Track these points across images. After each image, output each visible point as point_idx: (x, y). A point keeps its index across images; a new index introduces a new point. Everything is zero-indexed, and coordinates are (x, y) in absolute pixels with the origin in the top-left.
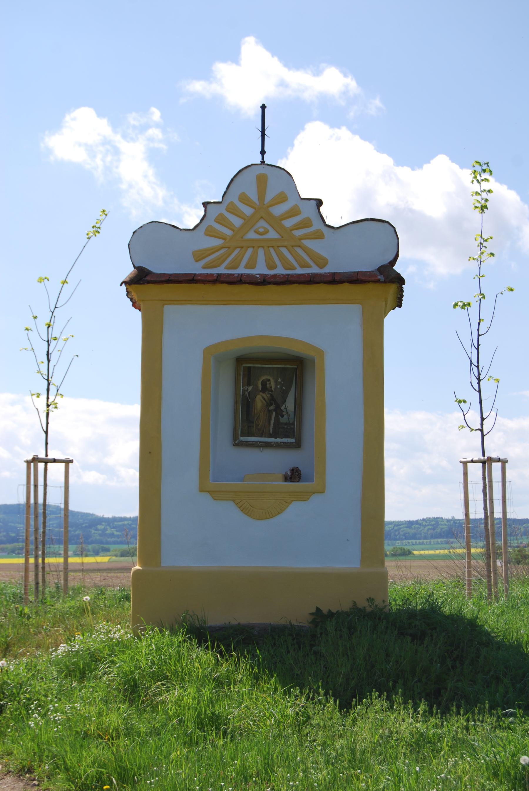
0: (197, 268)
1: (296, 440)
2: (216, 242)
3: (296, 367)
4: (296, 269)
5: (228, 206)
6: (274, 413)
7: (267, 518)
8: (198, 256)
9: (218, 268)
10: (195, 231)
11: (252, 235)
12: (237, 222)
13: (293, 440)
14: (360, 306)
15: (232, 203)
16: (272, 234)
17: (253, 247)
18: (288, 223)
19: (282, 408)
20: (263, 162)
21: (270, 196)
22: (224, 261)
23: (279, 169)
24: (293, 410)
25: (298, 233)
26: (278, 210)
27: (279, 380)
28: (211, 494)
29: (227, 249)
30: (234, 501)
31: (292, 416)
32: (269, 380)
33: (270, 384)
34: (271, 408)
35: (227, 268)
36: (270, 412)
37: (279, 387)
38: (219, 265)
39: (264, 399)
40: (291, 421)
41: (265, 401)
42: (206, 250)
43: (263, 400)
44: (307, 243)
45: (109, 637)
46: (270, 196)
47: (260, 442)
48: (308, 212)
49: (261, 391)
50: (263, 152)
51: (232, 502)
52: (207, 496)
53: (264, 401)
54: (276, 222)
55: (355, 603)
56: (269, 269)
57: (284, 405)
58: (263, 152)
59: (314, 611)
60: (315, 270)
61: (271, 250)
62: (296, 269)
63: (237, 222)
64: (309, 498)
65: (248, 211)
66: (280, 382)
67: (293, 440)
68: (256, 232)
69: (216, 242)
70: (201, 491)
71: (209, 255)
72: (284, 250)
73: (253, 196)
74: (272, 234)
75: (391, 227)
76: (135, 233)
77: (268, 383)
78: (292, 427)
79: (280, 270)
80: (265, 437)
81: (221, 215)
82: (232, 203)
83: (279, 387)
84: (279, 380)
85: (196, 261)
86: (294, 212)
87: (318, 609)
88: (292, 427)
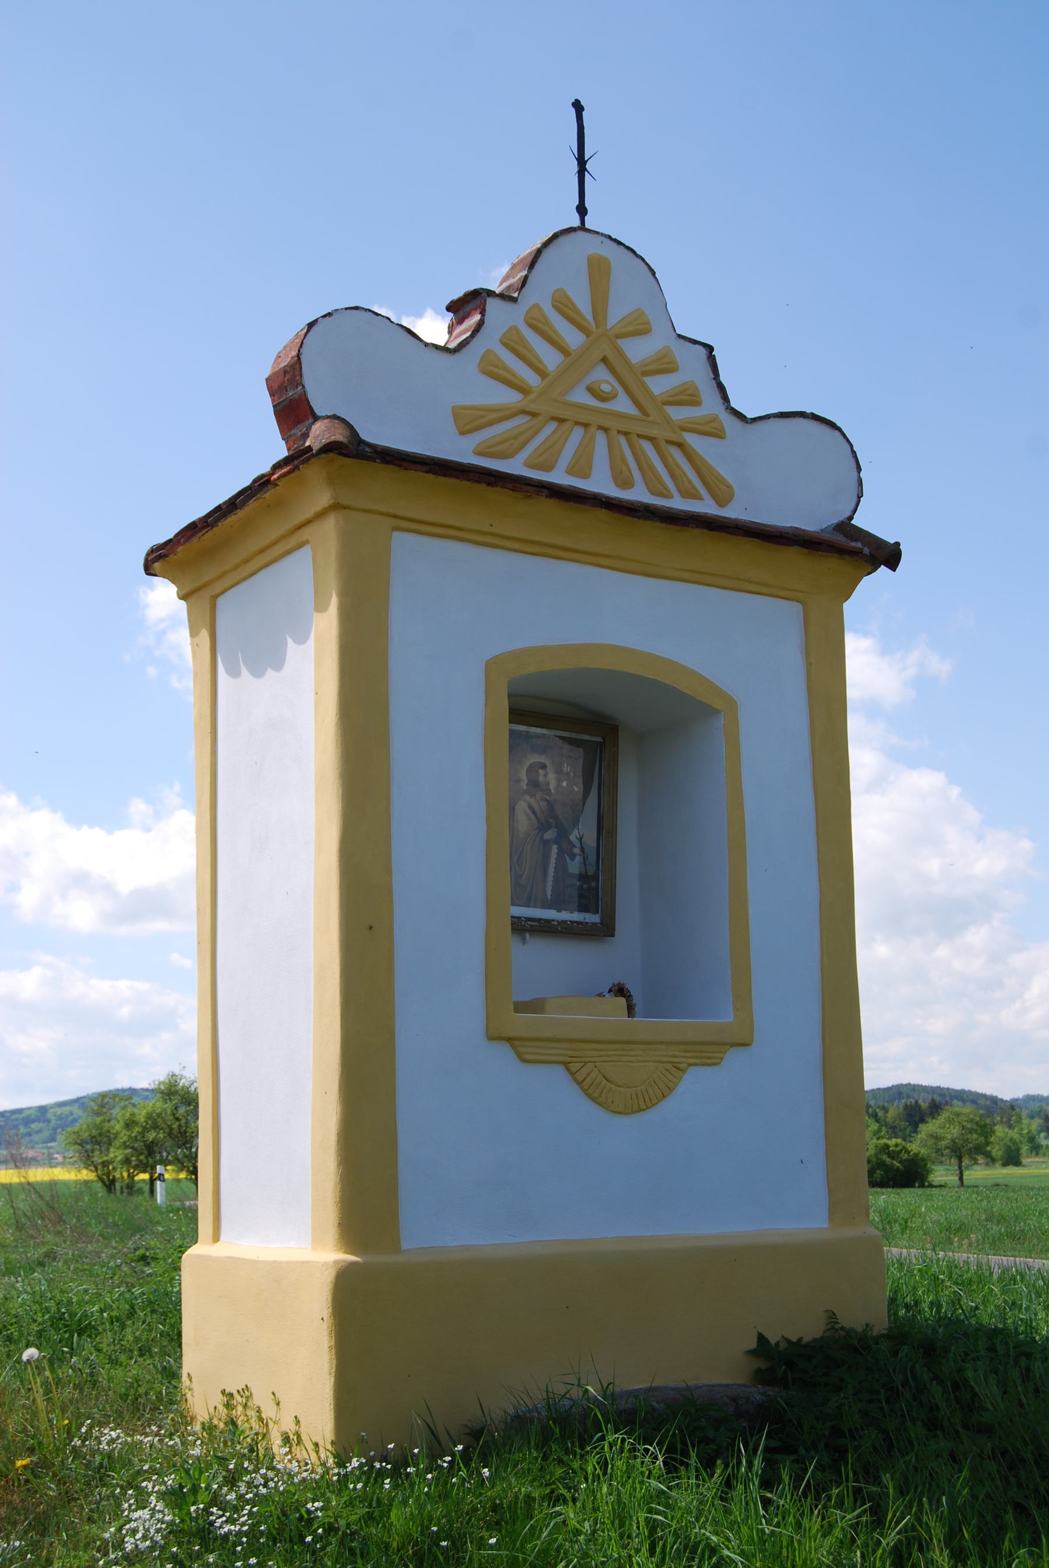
0: (461, 451)
1: (602, 918)
2: (509, 397)
3: (599, 739)
4: (672, 497)
5: (529, 311)
6: (555, 848)
7: (641, 1110)
8: (468, 421)
9: (507, 461)
10: (457, 355)
11: (581, 396)
12: (551, 359)
13: (593, 918)
14: (796, 608)
15: (536, 306)
16: (623, 405)
17: (586, 426)
18: (659, 385)
19: (572, 837)
20: (582, 227)
21: (616, 313)
22: (524, 445)
23: (631, 254)
24: (595, 845)
25: (678, 414)
26: (638, 351)
27: (566, 768)
28: (514, 1047)
29: (528, 418)
30: (566, 1064)
31: (592, 858)
32: (544, 766)
33: (545, 776)
34: (550, 835)
35: (528, 465)
36: (546, 844)
37: (564, 784)
38: (511, 456)
39: (534, 812)
40: (591, 871)
41: (537, 817)
42: (489, 409)
43: (529, 811)
44: (693, 440)
45: (247, 1482)
46: (616, 313)
47: (528, 919)
48: (691, 369)
49: (525, 792)
50: (582, 210)
51: (560, 1070)
52: (504, 1050)
53: (532, 816)
54: (629, 378)
55: (832, 1316)
56: (617, 485)
57: (576, 832)
58: (582, 210)
59: (753, 1344)
60: (707, 507)
61: (623, 440)
62: (672, 497)
63: (551, 359)
64: (722, 1059)
65: (573, 338)
66: (568, 774)
67: (593, 918)
68: (590, 390)
69: (509, 397)
70: (491, 1038)
71: (490, 424)
72: (647, 447)
73: (583, 304)
74: (623, 405)
75: (844, 441)
76: (315, 329)
77: (541, 772)
78: (593, 884)
79: (638, 494)
80: (535, 907)
81: (514, 329)
82: (536, 306)
83: (564, 784)
84: (566, 768)
85: (462, 433)
86: (664, 365)
87: (761, 1338)
88: (593, 884)
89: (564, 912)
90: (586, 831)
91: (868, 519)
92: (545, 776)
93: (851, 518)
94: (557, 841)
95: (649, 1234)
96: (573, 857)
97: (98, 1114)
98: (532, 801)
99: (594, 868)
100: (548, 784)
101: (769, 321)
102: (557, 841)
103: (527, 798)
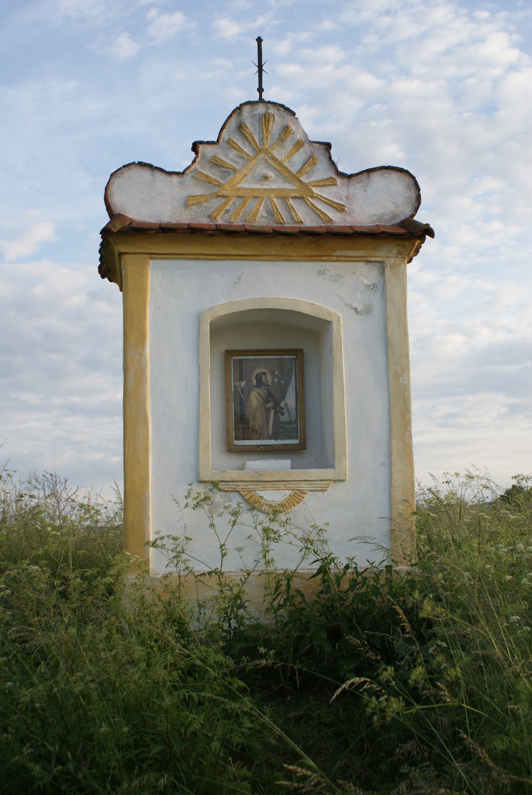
6: (272, 411)
19: (282, 405)
24: (295, 407)
32: (264, 374)
33: (265, 378)
34: (269, 405)
36: (268, 410)
37: (276, 380)
50: (260, 90)
55: (382, 464)
57: (284, 402)
58: (260, 90)
66: (278, 375)
77: (263, 376)
78: (295, 426)
80: (263, 439)
89: (279, 440)
90: (290, 400)
91: (421, 217)
92: (265, 378)
93: (413, 216)
94: (274, 407)
95: (242, 299)
96: (283, 414)
97: (46, 625)
98: (259, 391)
99: (295, 418)
100: (267, 381)
101: (354, 108)
102: (274, 407)
103: (256, 389)
